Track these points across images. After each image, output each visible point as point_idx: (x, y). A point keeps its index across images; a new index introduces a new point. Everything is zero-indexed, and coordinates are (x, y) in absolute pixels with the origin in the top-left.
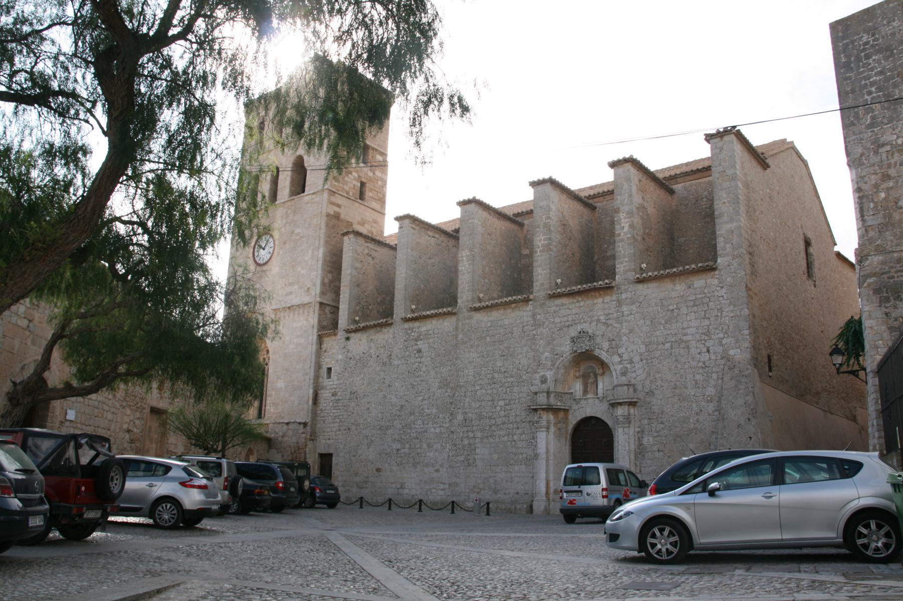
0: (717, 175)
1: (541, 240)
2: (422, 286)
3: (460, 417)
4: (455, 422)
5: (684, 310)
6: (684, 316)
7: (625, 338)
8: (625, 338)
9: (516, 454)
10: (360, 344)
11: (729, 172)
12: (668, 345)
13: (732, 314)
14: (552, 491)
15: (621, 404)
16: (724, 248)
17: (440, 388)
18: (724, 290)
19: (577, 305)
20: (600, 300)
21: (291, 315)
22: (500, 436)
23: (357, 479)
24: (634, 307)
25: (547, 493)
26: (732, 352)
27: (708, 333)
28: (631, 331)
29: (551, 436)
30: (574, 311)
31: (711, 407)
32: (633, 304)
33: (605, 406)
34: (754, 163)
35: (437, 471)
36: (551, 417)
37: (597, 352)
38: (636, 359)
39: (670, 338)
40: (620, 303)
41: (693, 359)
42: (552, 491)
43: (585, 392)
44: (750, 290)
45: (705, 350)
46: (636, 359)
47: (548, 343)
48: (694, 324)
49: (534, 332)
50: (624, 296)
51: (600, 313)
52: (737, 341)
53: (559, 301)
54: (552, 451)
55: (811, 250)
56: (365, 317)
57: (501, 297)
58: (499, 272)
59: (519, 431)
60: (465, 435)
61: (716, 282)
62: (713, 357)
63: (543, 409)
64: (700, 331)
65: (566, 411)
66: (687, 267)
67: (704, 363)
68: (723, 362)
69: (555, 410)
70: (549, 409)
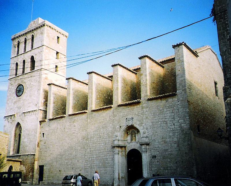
0: (177, 60)
1: (115, 86)
2: (76, 103)
3: (88, 150)
4: (87, 152)
5: (165, 110)
6: (165, 112)
7: (144, 120)
8: (144, 120)
9: (108, 163)
10: (55, 124)
11: (181, 59)
12: (160, 123)
13: (182, 111)
14: (120, 177)
15: (143, 144)
16: (179, 87)
17: (82, 139)
18: (179, 102)
19: (128, 108)
20: (136, 107)
21: (34, 113)
22: (102, 157)
23: (53, 175)
24: (147, 109)
25: (119, 178)
26: (182, 125)
27: (174, 118)
28: (147, 118)
29: (120, 156)
30: (127, 111)
31: (176, 145)
32: (147, 108)
33: (138, 145)
34: (192, 55)
35: (80, 170)
36: (120, 149)
37: (135, 125)
38: (149, 128)
39: (160, 120)
40: (143, 108)
41: (169, 128)
42: (120, 177)
43: (132, 140)
44: (189, 102)
45: (173, 124)
46: (149, 128)
47: (118, 123)
48: (169, 115)
49: (114, 118)
50: (144, 105)
51: (136, 111)
52: (184, 121)
53: (122, 107)
54: (120, 162)
55: (217, 86)
56: (58, 114)
57: (104, 106)
58: (103, 97)
59: (108, 155)
60: (90, 156)
61: (176, 99)
62: (176, 127)
63: (117, 147)
64: (171, 117)
65: (125, 147)
66: (166, 94)
67: (173, 129)
68: (179, 129)
69: (121, 147)
70: (119, 147)
